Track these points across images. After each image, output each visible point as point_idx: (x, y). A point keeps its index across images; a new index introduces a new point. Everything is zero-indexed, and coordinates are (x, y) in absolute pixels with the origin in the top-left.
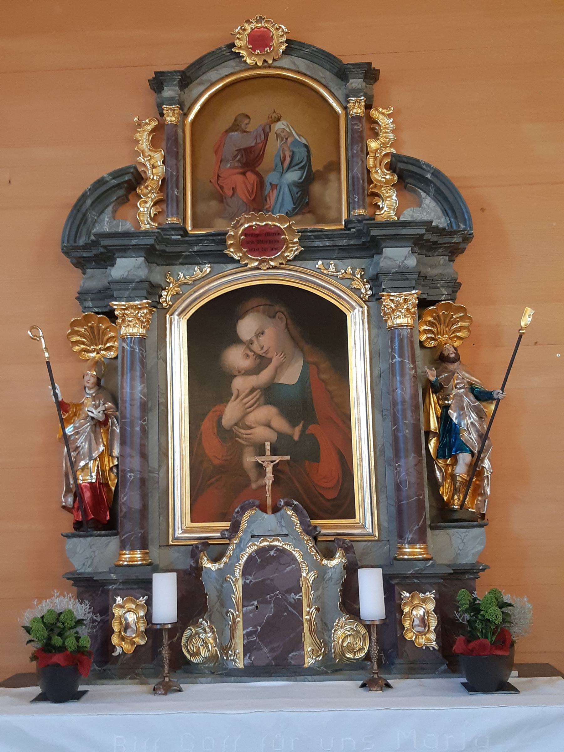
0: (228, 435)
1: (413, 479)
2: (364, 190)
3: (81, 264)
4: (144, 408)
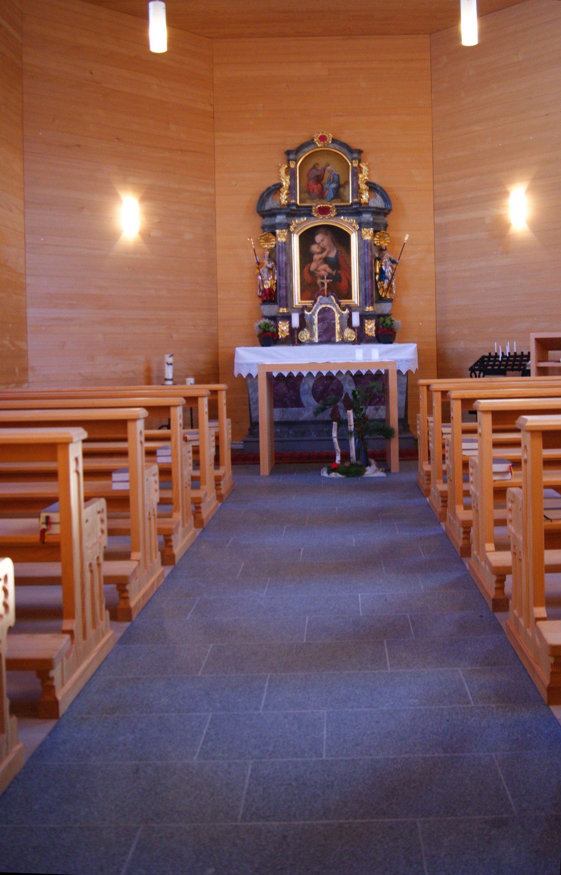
0: (312, 274)
1: (370, 287)
2: (357, 192)
3: (263, 216)
4: (286, 264)
